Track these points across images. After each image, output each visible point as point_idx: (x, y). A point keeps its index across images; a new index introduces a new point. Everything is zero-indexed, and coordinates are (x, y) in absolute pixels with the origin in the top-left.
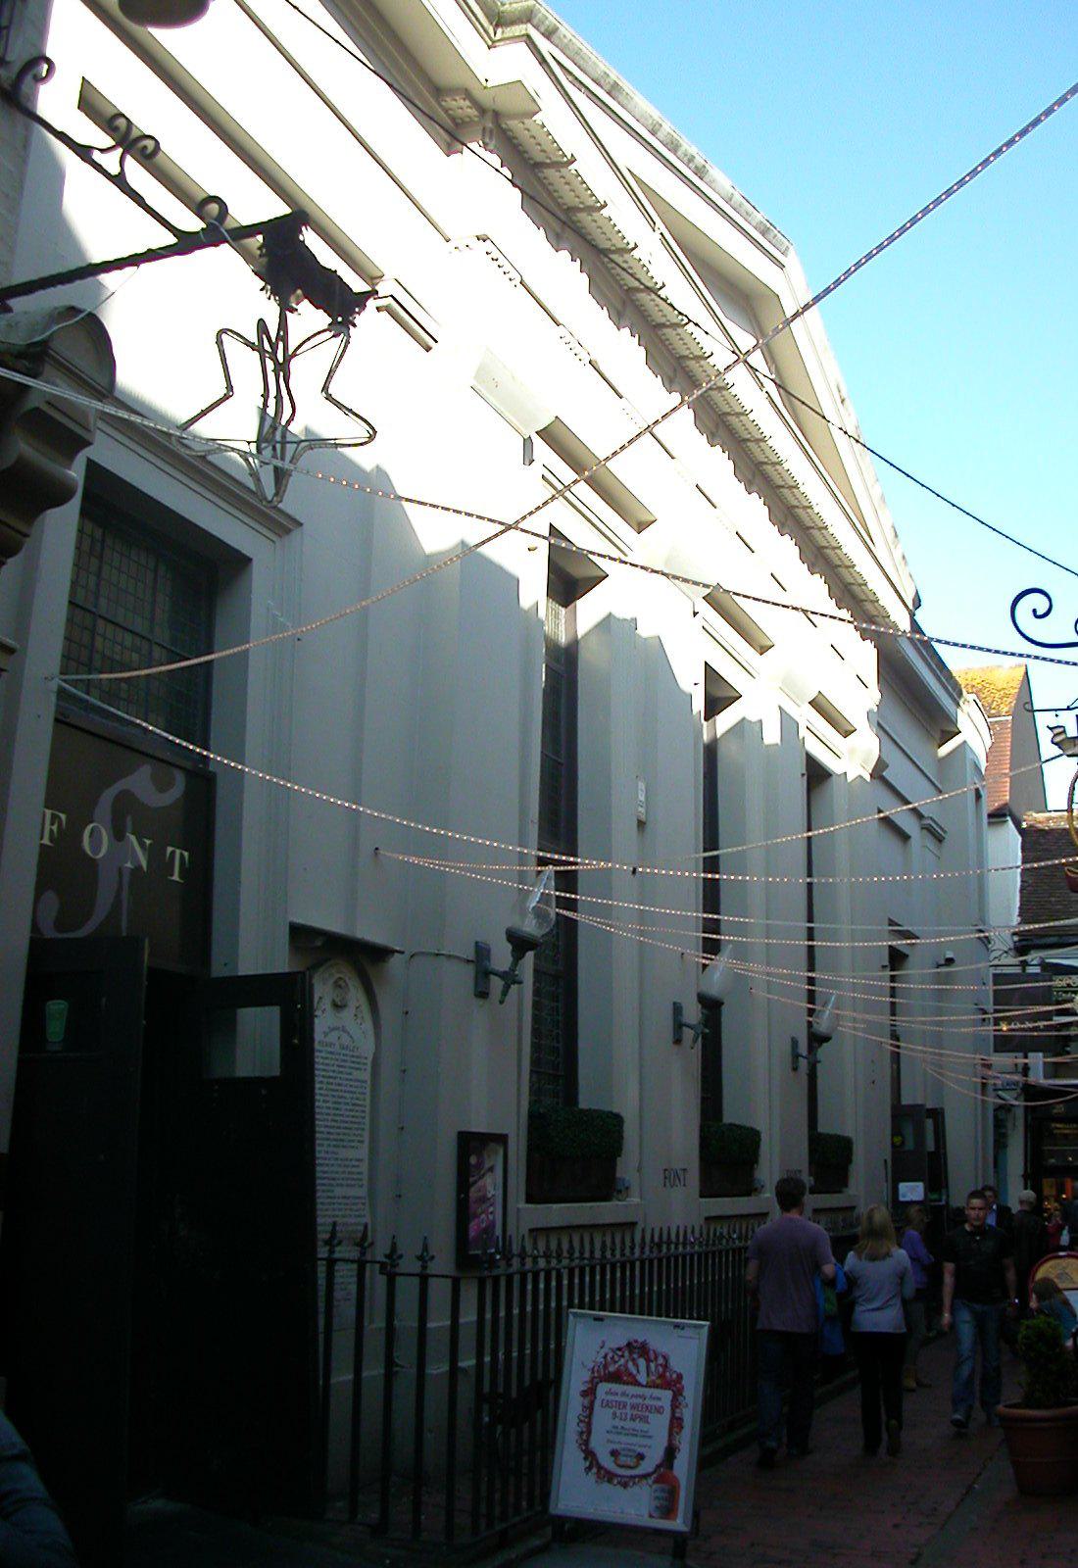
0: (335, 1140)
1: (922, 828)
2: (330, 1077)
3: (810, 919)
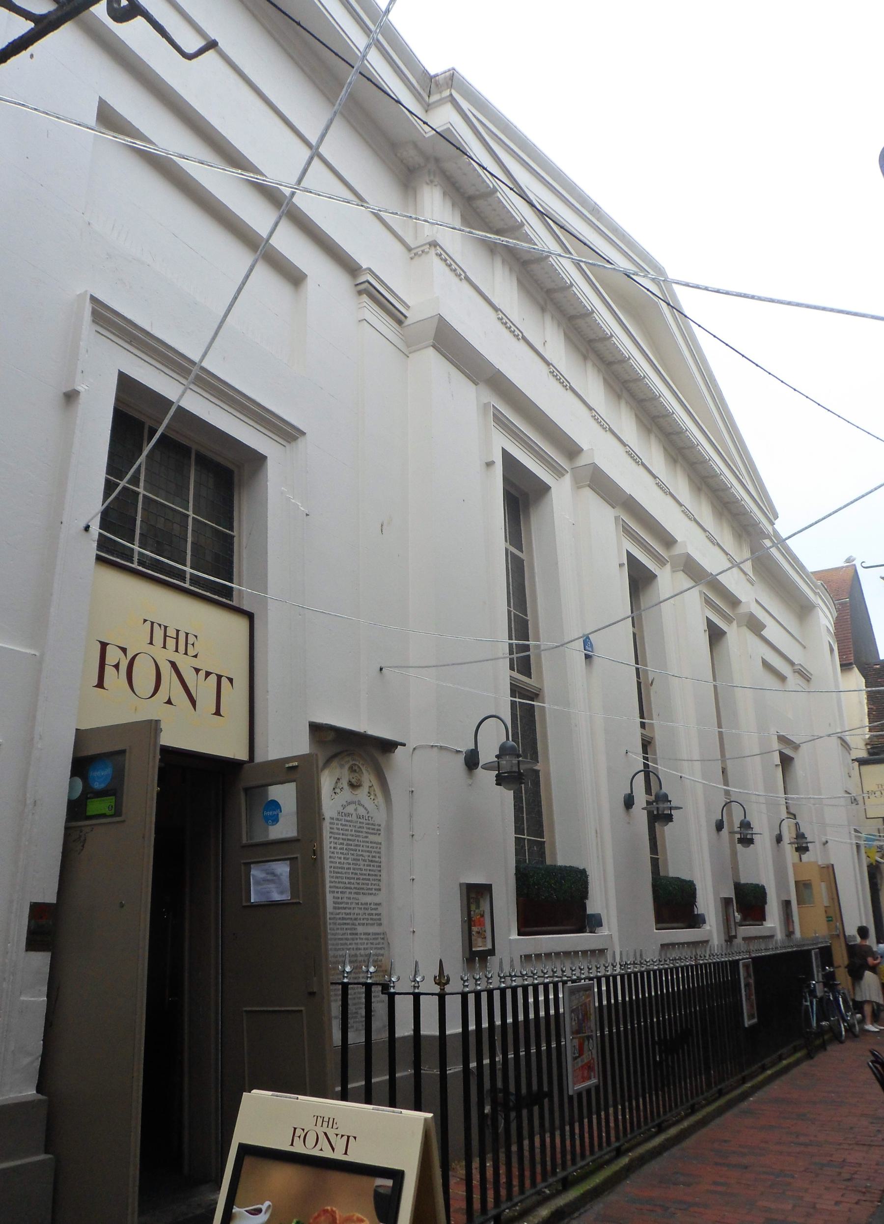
0: (355, 888)
1: (794, 672)
2: (348, 840)
3: (720, 726)
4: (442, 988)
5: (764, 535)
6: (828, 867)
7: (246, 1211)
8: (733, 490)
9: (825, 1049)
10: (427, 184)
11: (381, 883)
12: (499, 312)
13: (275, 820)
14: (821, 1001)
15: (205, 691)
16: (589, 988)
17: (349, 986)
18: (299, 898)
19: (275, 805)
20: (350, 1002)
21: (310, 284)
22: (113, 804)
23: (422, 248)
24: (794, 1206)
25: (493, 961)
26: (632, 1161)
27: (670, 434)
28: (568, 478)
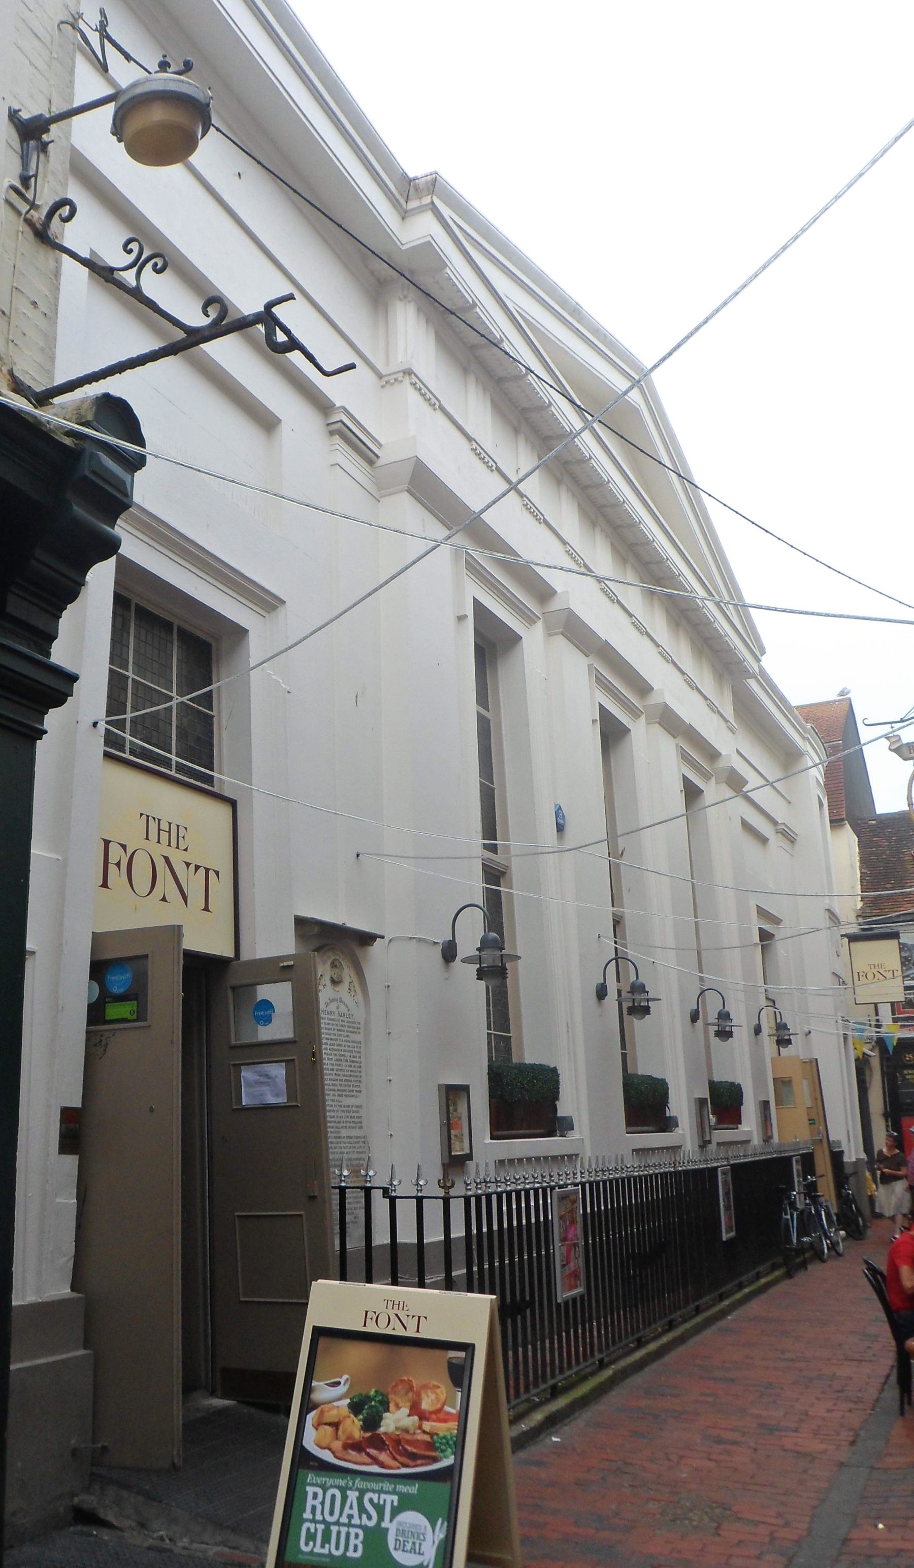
2: (332, 1039)
4: (447, 1191)
5: (747, 674)
6: (811, 1062)
7: (327, 1384)
8: (716, 625)
9: (806, 1268)
10: (401, 300)
11: (361, 1085)
12: (474, 443)
13: (268, 1020)
14: (801, 1213)
15: (194, 884)
16: (576, 1192)
17: (347, 1190)
18: (297, 1102)
19: (267, 1005)
20: (347, 1206)
21: (285, 429)
22: (135, 1009)
23: (395, 376)
24: (786, 1413)
25: (471, 1165)
26: (615, 1374)
27: (619, 527)
28: (540, 625)
